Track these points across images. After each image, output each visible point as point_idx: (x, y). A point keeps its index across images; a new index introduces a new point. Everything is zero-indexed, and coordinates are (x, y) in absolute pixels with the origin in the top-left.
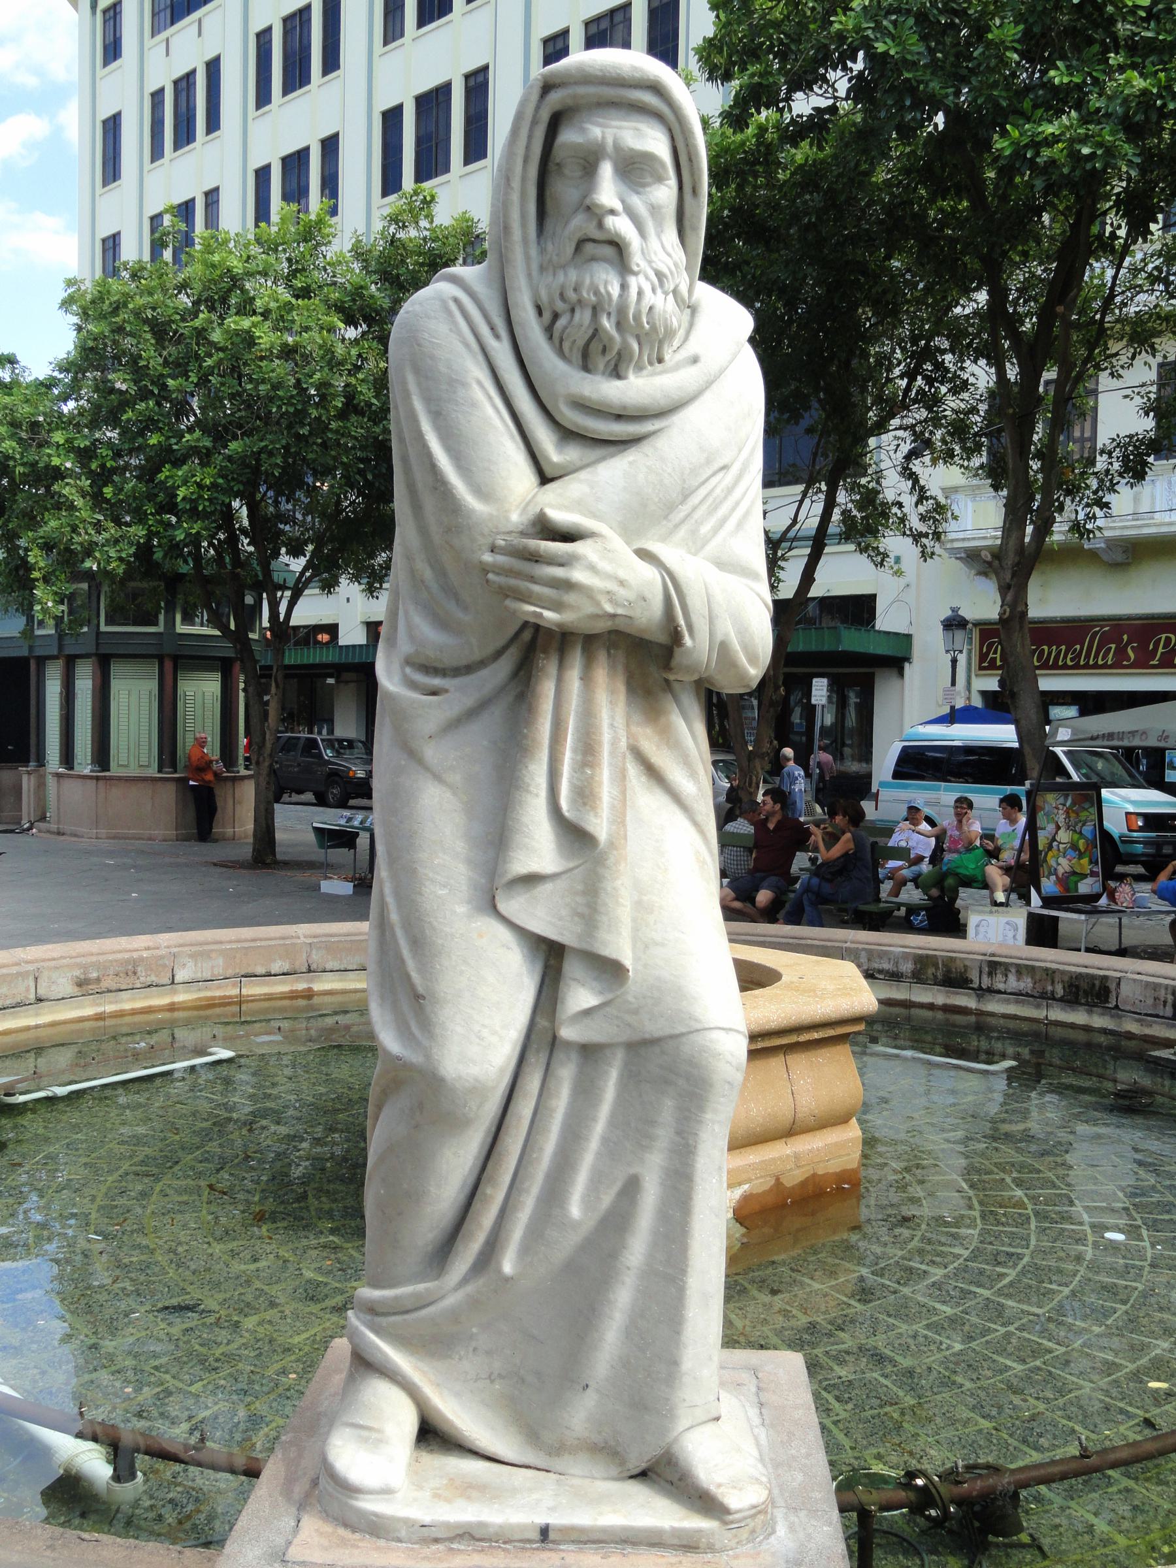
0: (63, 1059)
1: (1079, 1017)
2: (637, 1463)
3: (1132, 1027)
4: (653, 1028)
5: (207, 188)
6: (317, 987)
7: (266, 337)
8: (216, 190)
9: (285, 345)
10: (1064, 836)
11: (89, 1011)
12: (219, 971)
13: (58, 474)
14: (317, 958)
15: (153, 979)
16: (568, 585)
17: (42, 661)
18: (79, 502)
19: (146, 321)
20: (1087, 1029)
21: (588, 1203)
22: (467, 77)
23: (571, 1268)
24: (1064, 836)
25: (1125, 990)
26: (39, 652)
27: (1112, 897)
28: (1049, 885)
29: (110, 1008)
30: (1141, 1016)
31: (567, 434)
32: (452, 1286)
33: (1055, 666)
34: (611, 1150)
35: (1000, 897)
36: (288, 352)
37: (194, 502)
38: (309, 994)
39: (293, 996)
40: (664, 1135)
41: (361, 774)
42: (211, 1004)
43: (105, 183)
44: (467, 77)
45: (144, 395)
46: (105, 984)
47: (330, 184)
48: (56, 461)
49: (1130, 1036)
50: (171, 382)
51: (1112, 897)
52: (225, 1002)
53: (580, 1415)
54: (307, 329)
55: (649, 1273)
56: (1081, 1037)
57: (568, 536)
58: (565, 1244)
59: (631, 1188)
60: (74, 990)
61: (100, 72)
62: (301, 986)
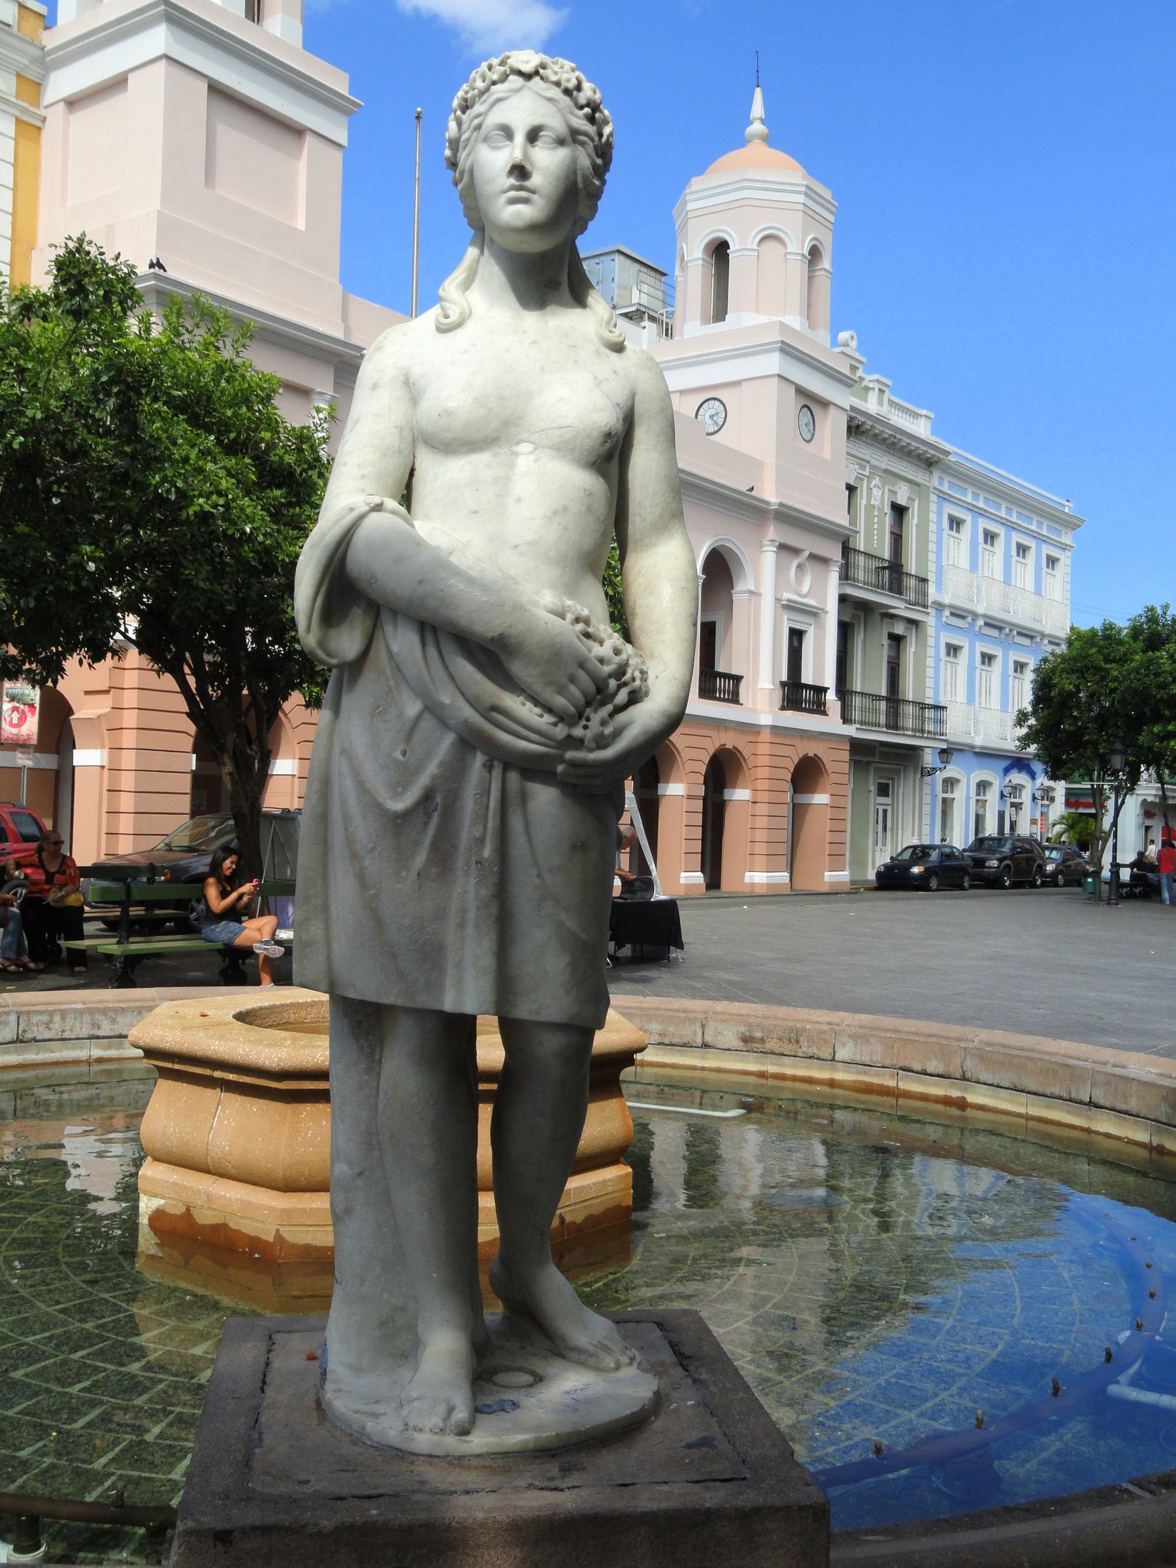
6: (971, 1098)
12: (877, 1058)
29: (772, 1069)
39: (947, 1101)
46: (771, 1045)
60: (735, 1043)
62: (955, 1094)
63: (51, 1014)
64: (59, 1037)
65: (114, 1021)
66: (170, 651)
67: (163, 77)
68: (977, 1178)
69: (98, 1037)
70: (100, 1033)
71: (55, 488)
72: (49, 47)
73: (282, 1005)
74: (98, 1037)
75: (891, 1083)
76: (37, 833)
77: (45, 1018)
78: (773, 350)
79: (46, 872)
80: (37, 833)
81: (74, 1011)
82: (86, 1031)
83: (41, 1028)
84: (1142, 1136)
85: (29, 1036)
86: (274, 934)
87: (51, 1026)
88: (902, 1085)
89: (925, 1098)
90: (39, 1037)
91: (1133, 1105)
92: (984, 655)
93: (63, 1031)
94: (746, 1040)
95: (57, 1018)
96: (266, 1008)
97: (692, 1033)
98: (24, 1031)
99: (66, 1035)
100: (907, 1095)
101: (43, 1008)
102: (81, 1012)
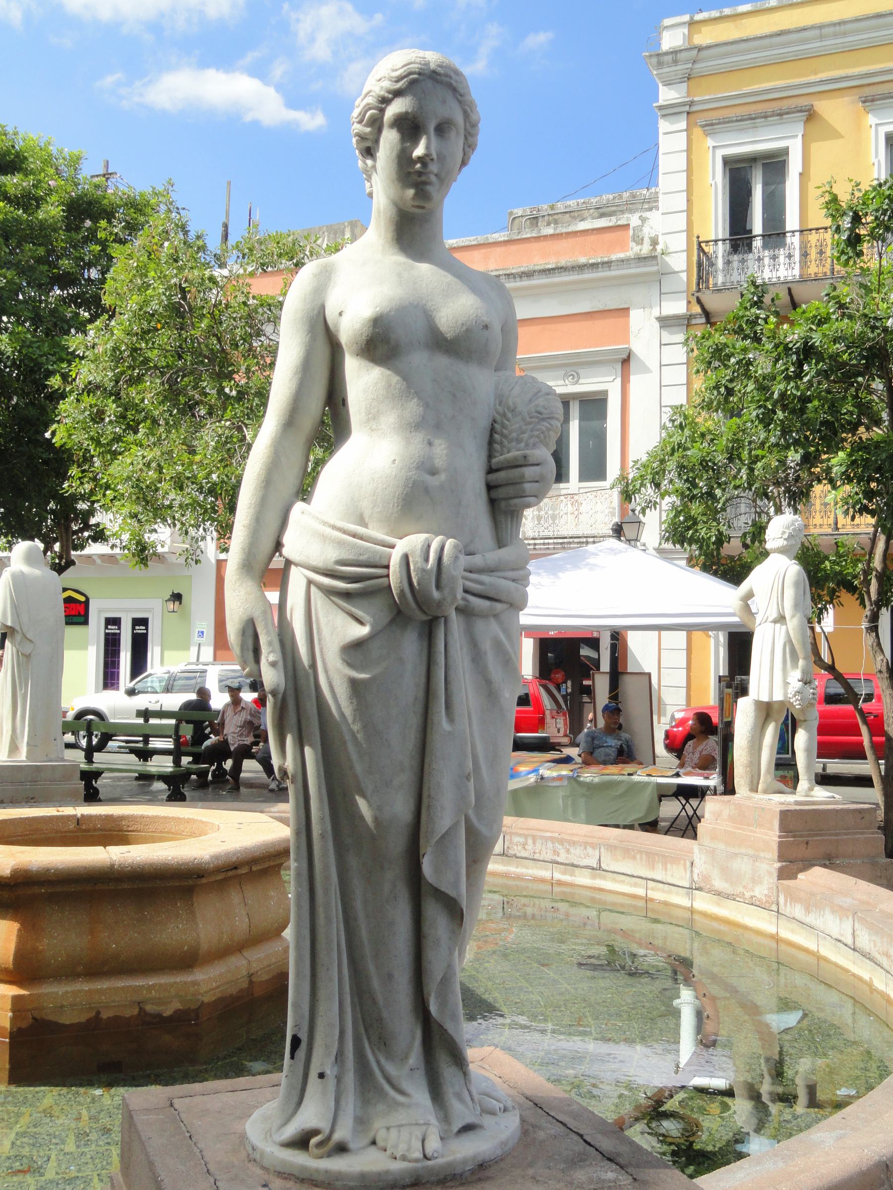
63: (526, 837)
64: (532, 857)
65: (568, 851)
68: (884, 241)
69: (558, 863)
70: (559, 859)
72: (171, 758)
73: (165, 818)
74: (558, 863)
76: (841, 690)
77: (522, 840)
78: (614, 361)
80: (841, 690)
81: (542, 837)
82: (549, 856)
83: (520, 848)
85: (511, 852)
87: (526, 847)
90: (518, 855)
92: (202, 632)
93: (534, 853)
95: (530, 841)
96: (148, 817)
98: (508, 848)
99: (537, 856)
101: (522, 832)
102: (547, 839)
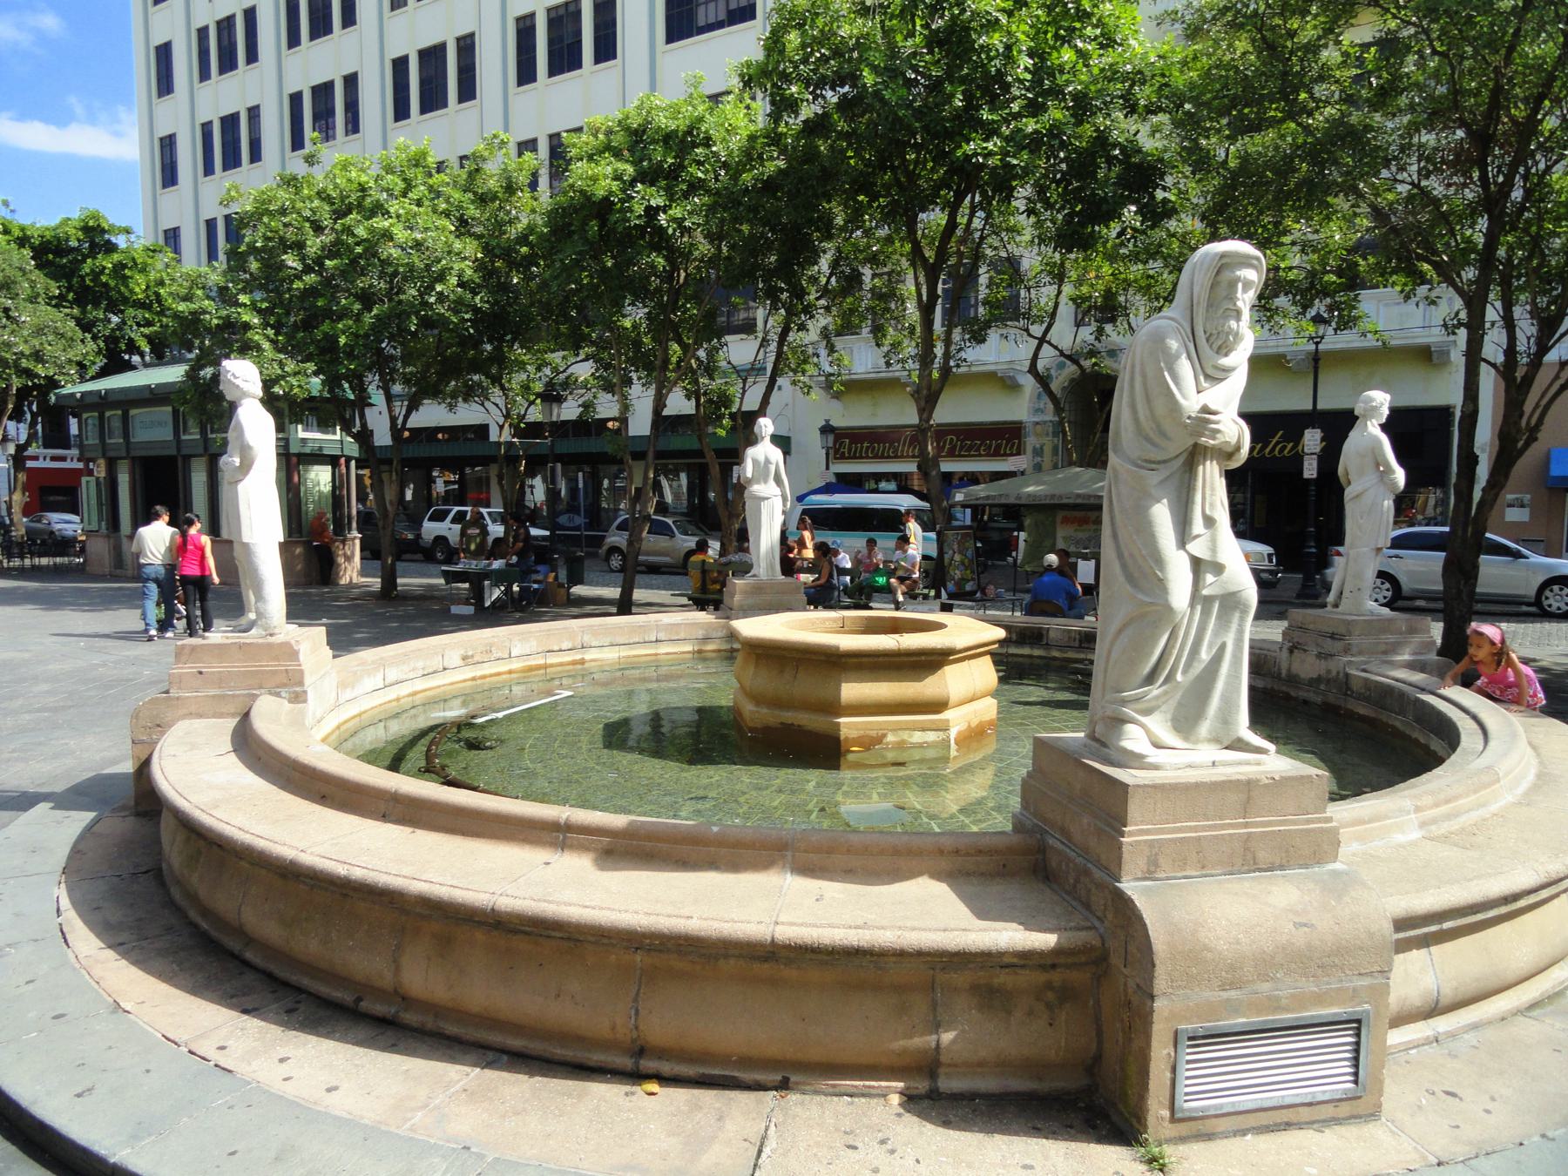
0: (458, 702)
1: (1026, 651)
2: (1226, 743)
3: (1056, 654)
4: (1233, 589)
5: (250, 105)
6: (587, 657)
7: (401, 234)
8: (258, 107)
9: (416, 240)
10: (957, 557)
11: (470, 675)
12: (534, 649)
13: (247, 326)
14: (587, 639)
15: (500, 655)
16: (1218, 431)
17: (187, 458)
18: (266, 345)
19: (308, 219)
20: (1031, 656)
21: (1208, 652)
22: (458, 40)
23: (1199, 678)
24: (957, 557)
25: (1052, 634)
26: (185, 451)
27: (983, 592)
28: (951, 586)
29: (479, 673)
30: (1061, 648)
31: (1207, 377)
32: (1155, 691)
33: (882, 457)
34: (1216, 634)
35: (901, 598)
36: (418, 245)
37: (352, 348)
38: (582, 662)
39: (574, 663)
40: (1234, 626)
41: (410, 536)
42: (531, 669)
43: (160, 95)
44: (458, 40)
45: (308, 270)
46: (476, 659)
47: (352, 107)
48: (246, 318)
49: (1055, 659)
50: (328, 262)
51: (983, 592)
52: (538, 667)
53: (1204, 728)
54: (427, 229)
55: (1229, 676)
56: (1027, 661)
57: (1215, 413)
58: (1198, 668)
59: (1223, 647)
60: (460, 663)
61: (152, 9)
62: (578, 657)
66: (263, 300)
67: (141, 973)
71: (265, 219)
75: (542, 662)
79: (1414, 24)
84: (689, 648)
86: (587, 240)
88: (1473, 797)
89: (561, 664)
91: (682, 636)
94: (464, 658)
97: (436, 663)
100: (552, 666)
